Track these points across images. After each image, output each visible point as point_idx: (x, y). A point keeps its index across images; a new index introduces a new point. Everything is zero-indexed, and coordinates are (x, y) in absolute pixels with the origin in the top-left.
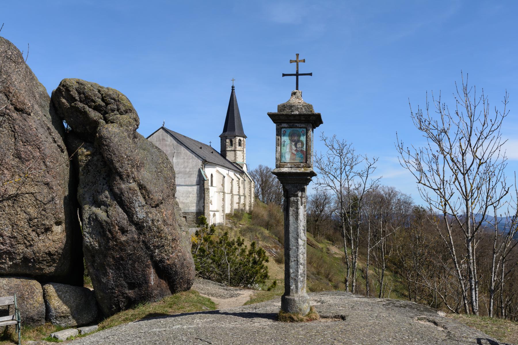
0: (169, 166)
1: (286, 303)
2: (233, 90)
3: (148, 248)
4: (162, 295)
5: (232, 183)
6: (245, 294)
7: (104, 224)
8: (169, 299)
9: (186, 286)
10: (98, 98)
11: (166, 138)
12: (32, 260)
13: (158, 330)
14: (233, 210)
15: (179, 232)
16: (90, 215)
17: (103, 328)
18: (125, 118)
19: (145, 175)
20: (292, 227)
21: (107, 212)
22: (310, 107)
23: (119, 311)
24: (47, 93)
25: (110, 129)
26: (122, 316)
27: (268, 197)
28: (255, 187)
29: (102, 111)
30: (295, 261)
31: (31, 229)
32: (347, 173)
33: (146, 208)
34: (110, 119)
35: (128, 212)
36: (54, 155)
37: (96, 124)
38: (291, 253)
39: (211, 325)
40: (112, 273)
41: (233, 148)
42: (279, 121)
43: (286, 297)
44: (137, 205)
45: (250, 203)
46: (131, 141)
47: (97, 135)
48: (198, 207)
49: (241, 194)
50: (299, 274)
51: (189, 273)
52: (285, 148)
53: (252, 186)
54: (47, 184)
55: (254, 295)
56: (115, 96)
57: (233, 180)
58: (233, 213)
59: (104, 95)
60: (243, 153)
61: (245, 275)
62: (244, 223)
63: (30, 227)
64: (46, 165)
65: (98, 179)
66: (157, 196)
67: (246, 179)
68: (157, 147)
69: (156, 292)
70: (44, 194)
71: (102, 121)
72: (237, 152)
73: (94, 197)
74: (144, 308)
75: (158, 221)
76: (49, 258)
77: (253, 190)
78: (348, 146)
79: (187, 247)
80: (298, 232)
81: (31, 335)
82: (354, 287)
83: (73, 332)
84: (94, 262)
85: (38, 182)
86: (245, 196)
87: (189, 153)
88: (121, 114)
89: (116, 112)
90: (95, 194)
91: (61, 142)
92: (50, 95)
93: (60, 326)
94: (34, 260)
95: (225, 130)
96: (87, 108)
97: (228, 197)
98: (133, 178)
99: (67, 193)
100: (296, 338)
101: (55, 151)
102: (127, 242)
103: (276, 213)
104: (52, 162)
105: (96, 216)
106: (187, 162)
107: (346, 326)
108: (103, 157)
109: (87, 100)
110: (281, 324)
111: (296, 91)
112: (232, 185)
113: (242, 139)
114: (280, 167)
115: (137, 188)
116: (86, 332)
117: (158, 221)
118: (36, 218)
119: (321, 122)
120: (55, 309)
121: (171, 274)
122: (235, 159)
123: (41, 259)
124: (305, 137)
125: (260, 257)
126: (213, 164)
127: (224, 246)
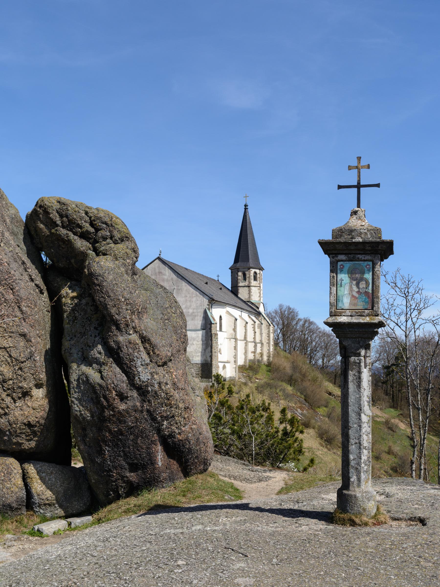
0: (178, 311)
1: (344, 500)
2: (246, 209)
3: (154, 419)
4: (172, 479)
5: (245, 327)
6: (278, 478)
7: (98, 388)
8: (181, 484)
9: (202, 467)
10: (85, 222)
11: (163, 271)
12: (8, 433)
13: (173, 531)
14: (248, 361)
15: (193, 398)
16: (79, 376)
17: (99, 521)
18: (121, 248)
19: (149, 324)
20: (353, 397)
21: (100, 372)
22: (377, 231)
23: (119, 499)
24: (20, 217)
25: (102, 263)
26: (122, 506)
27: (291, 344)
28: (275, 331)
29: (90, 239)
30: (356, 443)
31: (6, 393)
32: (415, 320)
33: (152, 368)
34: (101, 249)
35: (128, 372)
36: (31, 297)
37: (84, 256)
38: (351, 433)
39: (243, 527)
40: (108, 451)
41: (246, 283)
42: (334, 252)
43: (345, 492)
44: (139, 363)
45: (269, 353)
46: (129, 279)
47: (86, 270)
48: (205, 357)
49: (258, 340)
50: (362, 461)
51: (206, 451)
52: (342, 289)
53: (271, 331)
54: (24, 335)
55: (290, 479)
56: (107, 219)
57: (247, 323)
58: (247, 364)
59: (93, 218)
60: (260, 289)
61: (274, 452)
62: (262, 377)
63: (4, 391)
64: (21, 311)
65: (88, 328)
66: (165, 352)
67: (263, 321)
68: (162, 287)
69: (164, 475)
70: (20, 349)
71: (91, 253)
72: (252, 288)
73: (83, 353)
74: (150, 496)
75: (167, 384)
76: (29, 431)
77: (272, 335)
78: (416, 284)
79: (203, 416)
80: (360, 405)
81: (10, 527)
82: (422, 472)
83: (61, 524)
84: (85, 436)
85: (12, 332)
86: (262, 344)
87: (191, 290)
88: (115, 244)
89: (108, 240)
90: (84, 348)
91: (39, 281)
92: (24, 219)
93: (45, 516)
94: (10, 432)
95: (237, 260)
96: (72, 236)
97: (241, 345)
98: (133, 327)
99: (48, 346)
100: (365, 552)
101: (32, 292)
102: (127, 411)
103: (301, 365)
104: (29, 307)
105: (87, 377)
106: (190, 301)
107: (431, 535)
108: (94, 300)
109: (72, 225)
110: (339, 529)
111: (357, 209)
112: (246, 329)
113: (258, 271)
114: (335, 315)
115: (139, 341)
116: (77, 524)
117: (167, 384)
118: (11, 379)
119: (392, 253)
120: (38, 495)
121: (183, 452)
122: (249, 297)
123: (19, 431)
124: (371, 273)
125: (293, 428)
126: (223, 304)
127: (247, 413)
